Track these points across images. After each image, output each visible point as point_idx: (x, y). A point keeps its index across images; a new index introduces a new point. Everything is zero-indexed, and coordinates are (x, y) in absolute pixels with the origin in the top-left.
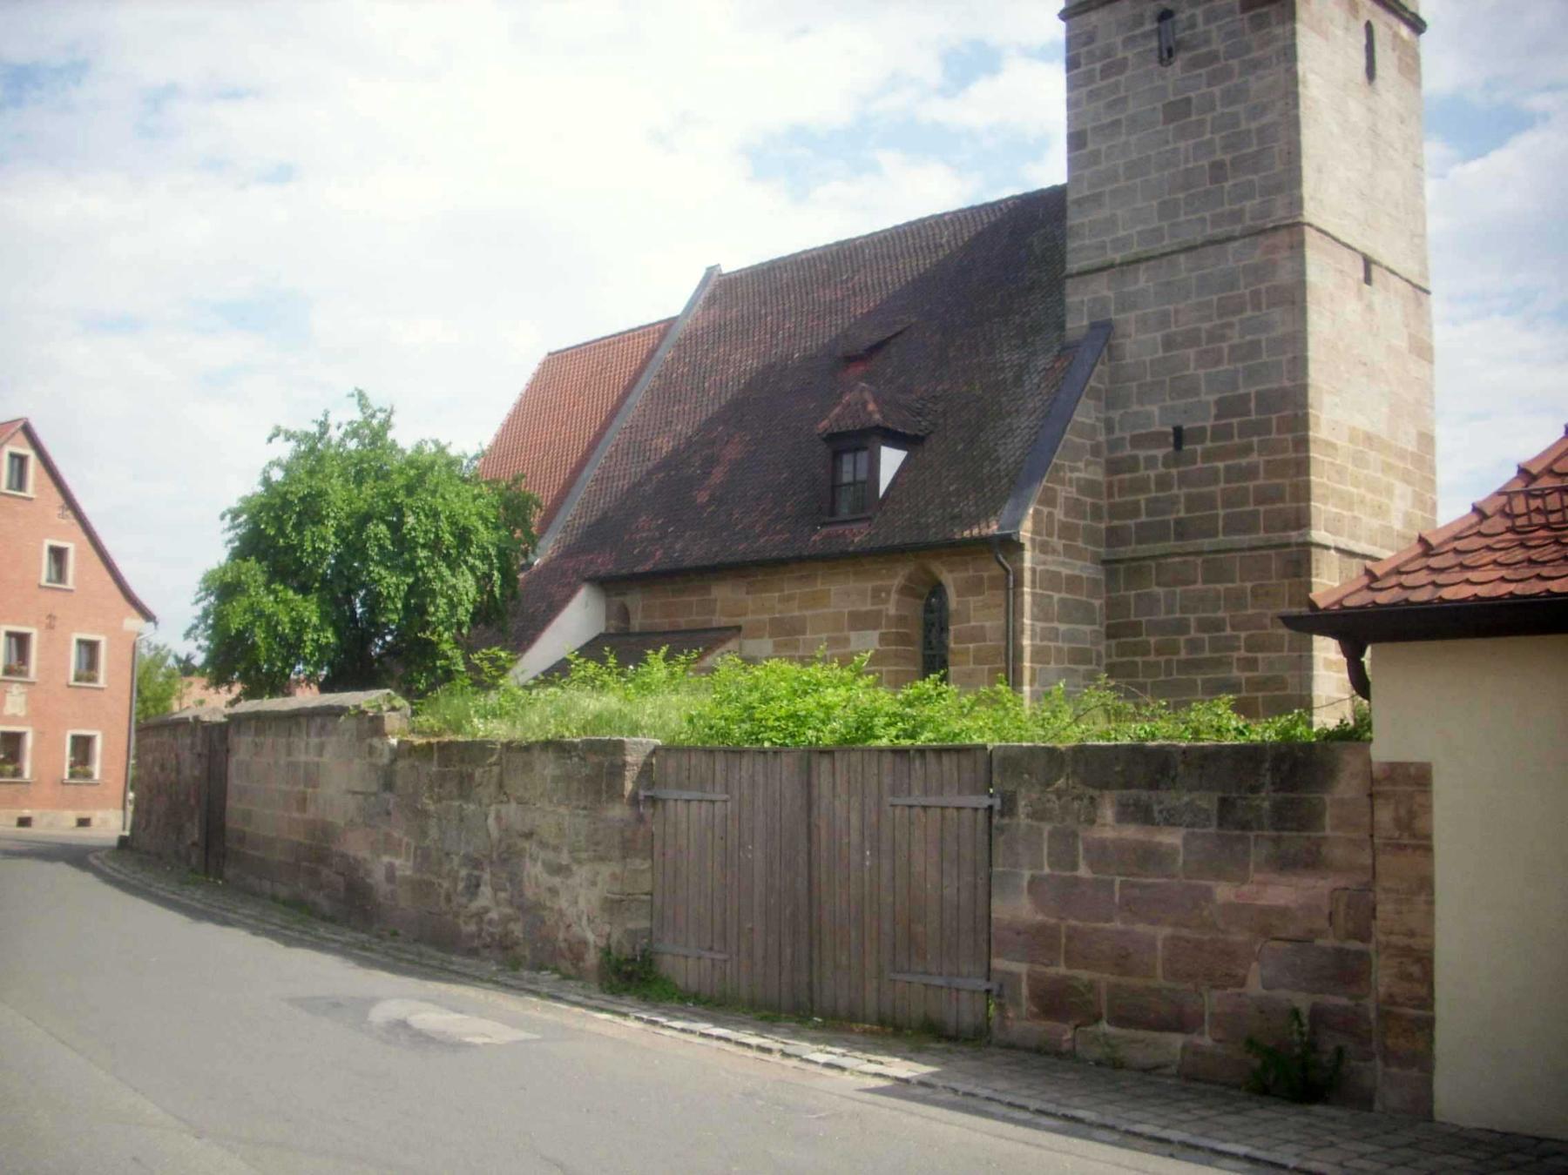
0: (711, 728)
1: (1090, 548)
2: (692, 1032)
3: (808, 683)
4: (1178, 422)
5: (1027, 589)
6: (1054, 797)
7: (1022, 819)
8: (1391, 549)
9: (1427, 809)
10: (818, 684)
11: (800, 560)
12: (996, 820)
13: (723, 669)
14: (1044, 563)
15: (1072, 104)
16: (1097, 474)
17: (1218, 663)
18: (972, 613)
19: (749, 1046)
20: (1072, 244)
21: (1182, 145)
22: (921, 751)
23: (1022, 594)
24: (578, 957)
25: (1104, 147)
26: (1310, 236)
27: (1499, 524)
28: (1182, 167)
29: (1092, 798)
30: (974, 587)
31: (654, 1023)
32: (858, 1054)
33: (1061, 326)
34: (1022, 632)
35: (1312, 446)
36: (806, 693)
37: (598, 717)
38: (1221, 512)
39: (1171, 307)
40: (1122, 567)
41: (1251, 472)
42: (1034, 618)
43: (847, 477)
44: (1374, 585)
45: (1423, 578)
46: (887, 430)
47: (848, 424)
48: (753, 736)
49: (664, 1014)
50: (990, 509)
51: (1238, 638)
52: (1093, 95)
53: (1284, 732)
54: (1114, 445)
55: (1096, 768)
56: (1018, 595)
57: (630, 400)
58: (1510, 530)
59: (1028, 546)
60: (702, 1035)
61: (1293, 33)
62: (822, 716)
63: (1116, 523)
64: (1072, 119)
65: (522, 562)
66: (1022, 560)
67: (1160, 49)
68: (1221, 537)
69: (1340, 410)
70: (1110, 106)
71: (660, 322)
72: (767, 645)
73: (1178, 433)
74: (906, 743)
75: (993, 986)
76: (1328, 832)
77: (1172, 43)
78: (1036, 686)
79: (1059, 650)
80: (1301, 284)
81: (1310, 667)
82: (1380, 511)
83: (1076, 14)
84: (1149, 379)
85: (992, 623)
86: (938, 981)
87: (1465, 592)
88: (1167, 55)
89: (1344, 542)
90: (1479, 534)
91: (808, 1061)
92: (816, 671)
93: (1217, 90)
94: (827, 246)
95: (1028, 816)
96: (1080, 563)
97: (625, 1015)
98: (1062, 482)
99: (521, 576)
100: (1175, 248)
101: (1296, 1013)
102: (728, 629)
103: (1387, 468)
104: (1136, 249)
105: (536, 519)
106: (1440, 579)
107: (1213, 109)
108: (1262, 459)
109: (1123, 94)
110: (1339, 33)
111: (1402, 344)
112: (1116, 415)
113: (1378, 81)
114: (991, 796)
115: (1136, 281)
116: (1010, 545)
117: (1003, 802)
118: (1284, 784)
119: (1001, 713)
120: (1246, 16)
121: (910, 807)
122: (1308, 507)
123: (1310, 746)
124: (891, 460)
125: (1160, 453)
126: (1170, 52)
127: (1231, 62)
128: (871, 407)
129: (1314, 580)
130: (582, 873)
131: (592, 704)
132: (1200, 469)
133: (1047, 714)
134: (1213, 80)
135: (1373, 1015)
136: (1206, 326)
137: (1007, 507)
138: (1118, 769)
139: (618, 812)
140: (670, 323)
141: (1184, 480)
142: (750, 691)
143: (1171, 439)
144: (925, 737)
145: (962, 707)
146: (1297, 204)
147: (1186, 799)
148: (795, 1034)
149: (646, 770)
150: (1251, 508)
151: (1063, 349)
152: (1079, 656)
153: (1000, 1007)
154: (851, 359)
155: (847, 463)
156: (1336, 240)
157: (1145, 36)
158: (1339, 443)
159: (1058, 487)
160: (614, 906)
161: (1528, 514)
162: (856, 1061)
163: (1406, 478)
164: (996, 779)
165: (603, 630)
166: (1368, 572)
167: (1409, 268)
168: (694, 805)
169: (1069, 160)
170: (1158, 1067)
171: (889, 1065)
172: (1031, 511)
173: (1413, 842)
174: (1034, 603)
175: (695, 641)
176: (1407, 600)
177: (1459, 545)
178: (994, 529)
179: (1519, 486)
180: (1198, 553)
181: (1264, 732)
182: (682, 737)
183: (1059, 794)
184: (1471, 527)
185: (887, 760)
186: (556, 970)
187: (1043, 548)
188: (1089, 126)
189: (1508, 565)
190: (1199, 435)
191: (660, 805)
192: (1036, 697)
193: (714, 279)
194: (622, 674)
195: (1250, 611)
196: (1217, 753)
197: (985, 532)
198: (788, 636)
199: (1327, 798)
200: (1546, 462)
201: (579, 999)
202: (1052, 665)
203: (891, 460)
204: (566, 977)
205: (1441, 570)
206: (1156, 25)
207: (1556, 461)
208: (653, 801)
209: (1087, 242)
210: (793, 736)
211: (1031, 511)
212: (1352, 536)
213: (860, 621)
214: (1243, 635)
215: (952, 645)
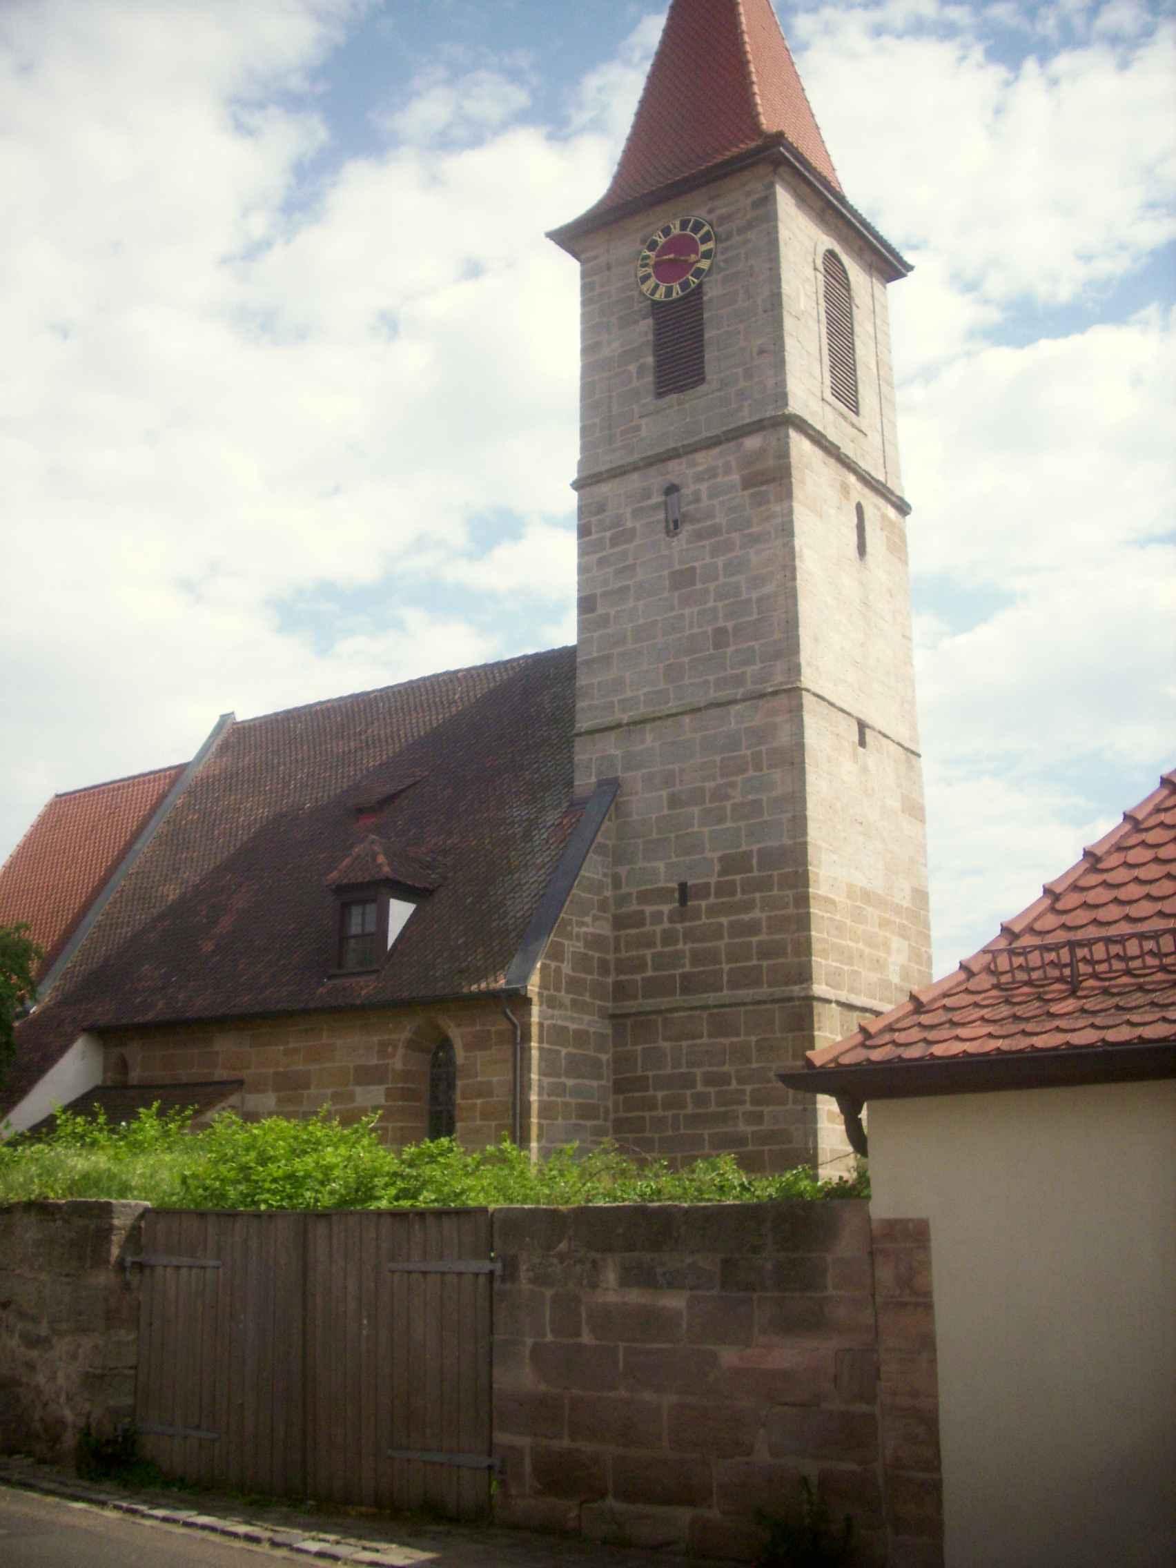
0: (206, 1189)
1: (598, 1002)
2: (174, 1521)
3: (307, 1142)
4: (682, 879)
5: (534, 1044)
6: (555, 1261)
7: (524, 1284)
8: (890, 1002)
9: (926, 1265)
10: (318, 1142)
11: (306, 1012)
12: (497, 1285)
13: (219, 1127)
14: (552, 1017)
15: (583, 569)
16: (604, 929)
17: (724, 1118)
18: (478, 1067)
19: (235, 1535)
20: (581, 704)
21: (687, 611)
22: (422, 1214)
23: (530, 1049)
24: (56, 1439)
25: (612, 613)
26: (807, 699)
27: (985, 981)
28: (687, 633)
29: (594, 1262)
30: (479, 1042)
31: (134, 1512)
32: (352, 1541)
33: (570, 784)
34: (530, 1088)
35: (812, 902)
36: (305, 1152)
37: (86, 1176)
38: (726, 967)
39: (676, 767)
40: (629, 1022)
41: (753, 928)
42: (542, 1073)
43: (355, 929)
44: (868, 1043)
45: (915, 1034)
46: (398, 883)
47: (360, 877)
48: (249, 1198)
49: (144, 1502)
50: (498, 963)
51: (743, 1092)
52: (601, 562)
53: (785, 1189)
54: (622, 900)
55: (597, 1230)
56: (526, 1050)
57: (137, 846)
58: (997, 986)
59: (535, 999)
60: (187, 1524)
61: (790, 512)
62: (320, 1176)
63: (622, 977)
64: (581, 586)
65: (19, 1009)
66: (530, 1015)
67: (667, 521)
68: (725, 992)
69: (841, 864)
70: (619, 572)
71: (170, 768)
72: (269, 1100)
73: (683, 887)
74: (406, 1204)
75: (496, 1461)
76: (831, 1291)
77: (677, 516)
78: (544, 1142)
79: (566, 1104)
80: (799, 747)
81: (814, 1120)
82: (879, 965)
83: (590, 485)
84: (655, 836)
85: (498, 1077)
86: (438, 1457)
87: (956, 1048)
88: (673, 527)
89: (844, 996)
90: (967, 991)
91: (300, 1551)
92: (317, 1130)
93: (720, 561)
94: (341, 699)
95: (531, 1281)
96: (587, 1018)
97: (103, 1504)
98: (569, 936)
99: (16, 1024)
100: (680, 710)
101: (804, 1481)
102: (232, 1082)
103: (884, 923)
104: (642, 710)
105: (34, 966)
106: (931, 1035)
107: (716, 579)
108: (764, 915)
109: (630, 561)
110: (832, 511)
111: (895, 803)
112: (623, 870)
113: (868, 557)
114: (492, 1260)
115: (643, 741)
116: (519, 1000)
117: (504, 1266)
118: (791, 1240)
119: (506, 1172)
120: (746, 493)
121: (410, 1272)
122: (810, 961)
123: (809, 1206)
124: (400, 912)
125: (666, 908)
126: (676, 527)
127: (733, 535)
128: (381, 859)
129: (816, 1033)
130: (62, 1346)
131: (77, 1163)
132: (704, 924)
133: (554, 1173)
134: (715, 552)
135: (881, 1481)
136: (710, 785)
137: (516, 960)
138: (620, 1231)
139: (103, 1278)
140: (181, 769)
141: (689, 936)
142: (247, 1150)
143: (677, 895)
144: (427, 1199)
145: (466, 1166)
146: (795, 670)
147: (689, 1260)
148: (288, 1522)
149: (135, 1234)
150: (755, 962)
151: (571, 805)
152: (586, 1112)
153: (503, 1484)
154: (360, 811)
155: (356, 913)
156: (832, 704)
157: (655, 508)
158: (837, 899)
159: (566, 942)
160: (94, 1381)
161: (1012, 971)
162: (352, 1549)
163: (903, 933)
164: (497, 1242)
165: (99, 1082)
166: (863, 1030)
167: (900, 731)
168: (184, 1271)
169: (579, 622)
170: (669, 1544)
171: (385, 1552)
172: (539, 965)
173: (913, 1299)
174: (541, 1058)
175: (192, 1097)
176: (899, 1057)
177: (948, 1002)
178: (502, 983)
179: (1003, 944)
180: (704, 1008)
181: (766, 1188)
182: (174, 1198)
183: (562, 1257)
184: (959, 984)
185: (387, 1222)
186: (29, 1454)
187: (550, 1002)
188: (599, 591)
189: (995, 1022)
190: (703, 891)
191: (147, 1272)
192: (545, 1153)
193: (229, 721)
194: (113, 1131)
195: (754, 1066)
196: (721, 1213)
197: (493, 986)
198: (293, 1095)
199: (829, 1258)
200: (1069, 881)
201: (52, 1486)
202: (560, 1121)
203: (400, 912)
204: (42, 1461)
205: (932, 1027)
206: (661, 499)
207: (1036, 919)
208: (140, 1267)
209: (596, 702)
210: (290, 1197)
211: (539, 965)
212: (852, 990)
213: (366, 1076)
214: (748, 1088)
215: (459, 1101)
